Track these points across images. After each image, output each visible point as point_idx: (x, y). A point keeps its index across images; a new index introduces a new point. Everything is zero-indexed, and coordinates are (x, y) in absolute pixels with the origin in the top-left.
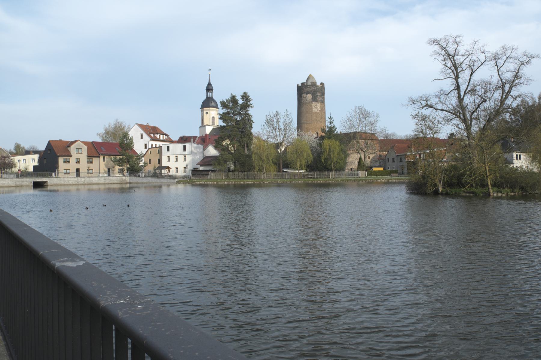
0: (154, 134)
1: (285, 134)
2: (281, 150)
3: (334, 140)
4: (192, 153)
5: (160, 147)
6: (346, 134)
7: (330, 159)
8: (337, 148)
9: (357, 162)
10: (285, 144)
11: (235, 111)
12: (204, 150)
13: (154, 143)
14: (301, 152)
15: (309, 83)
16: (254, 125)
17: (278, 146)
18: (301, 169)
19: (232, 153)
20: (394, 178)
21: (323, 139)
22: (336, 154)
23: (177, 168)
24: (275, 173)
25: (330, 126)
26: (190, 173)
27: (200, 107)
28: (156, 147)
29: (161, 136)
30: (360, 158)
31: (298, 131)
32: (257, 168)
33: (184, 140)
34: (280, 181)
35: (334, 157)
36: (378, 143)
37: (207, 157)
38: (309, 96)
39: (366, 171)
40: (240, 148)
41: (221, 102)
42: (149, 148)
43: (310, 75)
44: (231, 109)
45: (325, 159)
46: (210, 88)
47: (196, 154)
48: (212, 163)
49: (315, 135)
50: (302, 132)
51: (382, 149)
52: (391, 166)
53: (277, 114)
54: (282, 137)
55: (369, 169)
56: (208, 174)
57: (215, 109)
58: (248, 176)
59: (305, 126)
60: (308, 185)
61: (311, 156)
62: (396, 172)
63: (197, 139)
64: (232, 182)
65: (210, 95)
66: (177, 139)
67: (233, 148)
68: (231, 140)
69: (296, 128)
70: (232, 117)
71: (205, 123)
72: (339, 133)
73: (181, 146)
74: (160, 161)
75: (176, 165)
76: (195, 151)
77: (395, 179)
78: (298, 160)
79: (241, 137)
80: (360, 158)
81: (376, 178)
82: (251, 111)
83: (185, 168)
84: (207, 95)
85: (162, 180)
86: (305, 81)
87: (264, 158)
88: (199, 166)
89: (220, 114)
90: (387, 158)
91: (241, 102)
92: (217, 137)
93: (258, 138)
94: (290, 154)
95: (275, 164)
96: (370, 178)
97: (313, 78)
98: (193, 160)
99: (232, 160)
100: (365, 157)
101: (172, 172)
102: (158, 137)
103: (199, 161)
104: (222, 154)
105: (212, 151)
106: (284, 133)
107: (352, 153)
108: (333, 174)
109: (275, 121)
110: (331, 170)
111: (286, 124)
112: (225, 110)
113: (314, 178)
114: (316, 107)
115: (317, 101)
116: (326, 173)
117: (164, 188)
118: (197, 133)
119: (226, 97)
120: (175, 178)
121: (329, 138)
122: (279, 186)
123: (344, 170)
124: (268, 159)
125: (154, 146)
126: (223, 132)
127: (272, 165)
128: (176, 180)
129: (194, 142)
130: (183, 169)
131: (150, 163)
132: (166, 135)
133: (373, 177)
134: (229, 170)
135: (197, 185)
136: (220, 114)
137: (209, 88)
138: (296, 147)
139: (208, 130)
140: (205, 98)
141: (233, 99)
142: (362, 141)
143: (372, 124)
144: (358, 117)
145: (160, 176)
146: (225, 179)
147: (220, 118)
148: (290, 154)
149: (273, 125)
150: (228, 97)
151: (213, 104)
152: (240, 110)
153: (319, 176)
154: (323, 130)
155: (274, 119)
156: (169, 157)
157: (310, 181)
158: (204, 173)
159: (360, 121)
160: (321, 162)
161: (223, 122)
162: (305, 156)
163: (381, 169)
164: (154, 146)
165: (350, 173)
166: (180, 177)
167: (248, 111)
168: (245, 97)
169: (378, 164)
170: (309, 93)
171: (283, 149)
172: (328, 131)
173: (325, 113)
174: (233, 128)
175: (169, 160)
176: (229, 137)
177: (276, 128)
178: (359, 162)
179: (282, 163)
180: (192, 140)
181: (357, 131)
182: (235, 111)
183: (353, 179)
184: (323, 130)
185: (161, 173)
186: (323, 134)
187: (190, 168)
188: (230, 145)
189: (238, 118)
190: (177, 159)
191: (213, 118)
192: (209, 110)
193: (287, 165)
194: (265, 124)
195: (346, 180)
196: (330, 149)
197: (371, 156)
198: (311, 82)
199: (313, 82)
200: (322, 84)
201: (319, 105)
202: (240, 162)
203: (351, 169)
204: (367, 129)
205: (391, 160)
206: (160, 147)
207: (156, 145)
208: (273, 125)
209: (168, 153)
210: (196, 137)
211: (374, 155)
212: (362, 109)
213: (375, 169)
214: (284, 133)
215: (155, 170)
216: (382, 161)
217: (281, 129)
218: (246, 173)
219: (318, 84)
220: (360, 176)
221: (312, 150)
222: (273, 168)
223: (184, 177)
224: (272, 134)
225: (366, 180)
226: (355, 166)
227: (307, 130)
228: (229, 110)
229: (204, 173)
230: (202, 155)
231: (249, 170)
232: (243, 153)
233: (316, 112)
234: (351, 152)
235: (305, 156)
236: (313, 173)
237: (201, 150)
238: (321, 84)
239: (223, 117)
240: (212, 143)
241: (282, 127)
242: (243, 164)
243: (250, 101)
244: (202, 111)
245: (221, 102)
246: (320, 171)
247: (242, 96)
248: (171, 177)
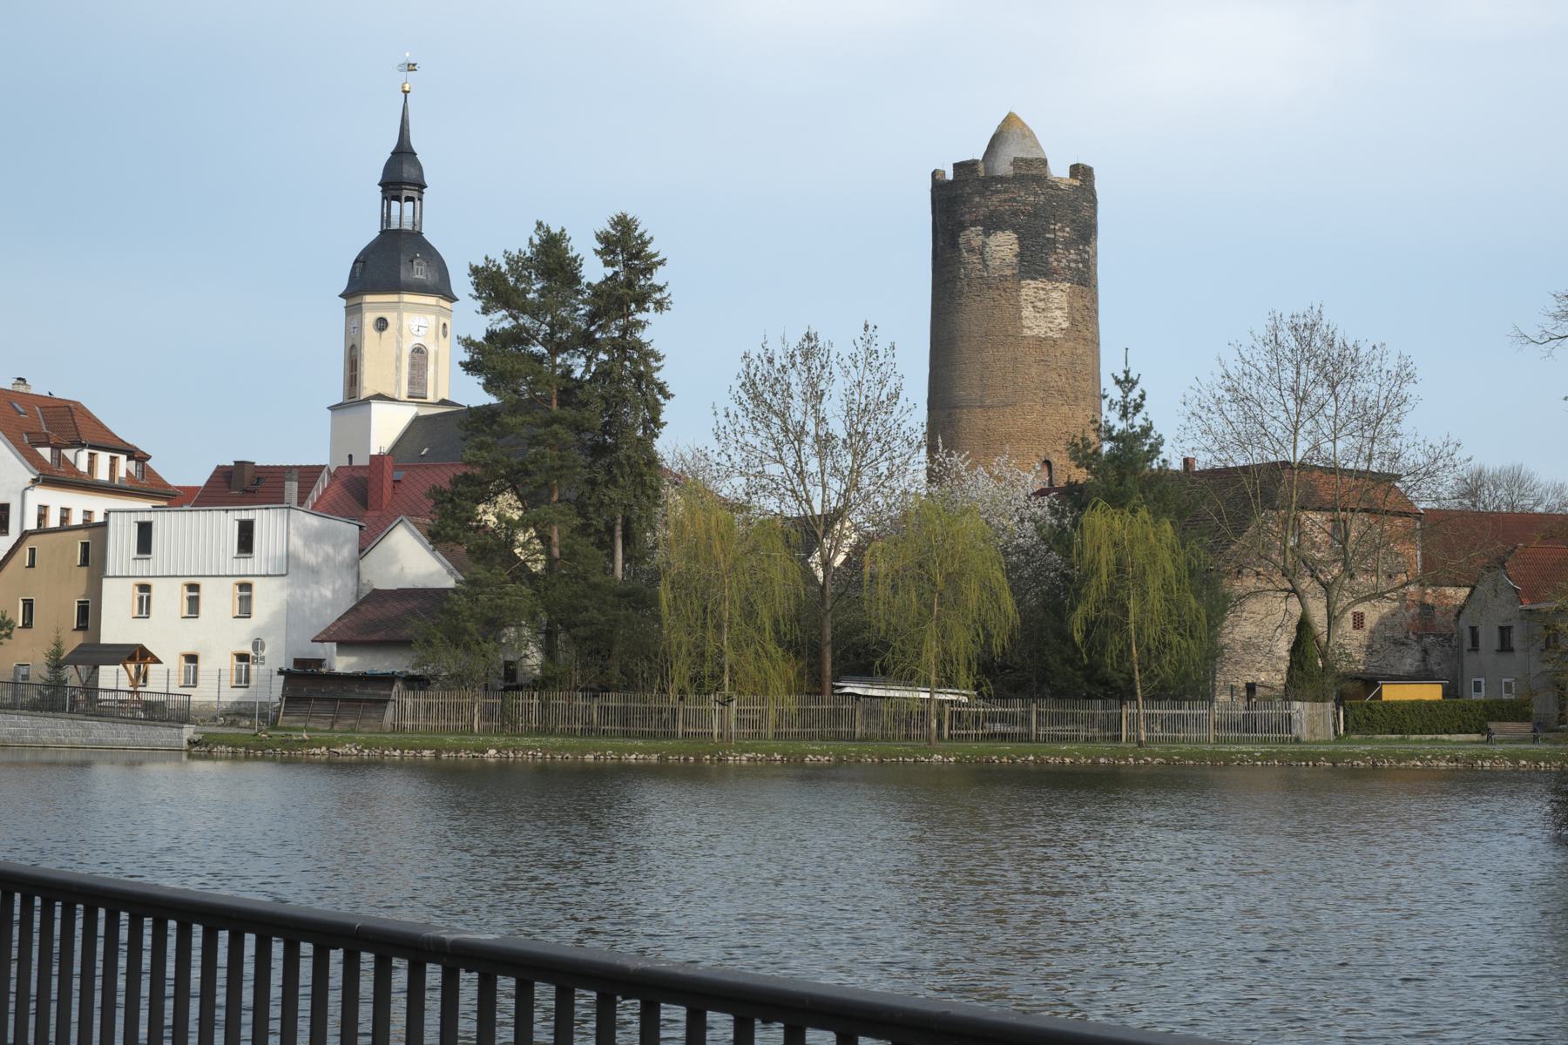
0: (56, 448)
1: (856, 472)
2: (826, 564)
3: (1143, 513)
4: (290, 567)
5: (97, 530)
6: (1223, 477)
7: (1121, 627)
8: (1165, 556)
9: (1283, 647)
10: (857, 528)
11: (558, 325)
12: (363, 549)
13: (56, 499)
14: (948, 577)
15: (1004, 167)
16: (669, 412)
17: (809, 532)
18: (949, 682)
19: (533, 577)
20: (1506, 745)
21: (1080, 505)
22: (1155, 597)
23: (192, 658)
24: (791, 704)
25: (1120, 426)
26: (268, 688)
27: (343, 284)
28: (65, 526)
29: (103, 458)
30: (1304, 625)
31: (932, 450)
32: (681, 671)
33: (241, 486)
34: (818, 754)
35: (1145, 611)
36: (1408, 537)
37: (378, 596)
38: (1004, 246)
39: (1339, 702)
40: (585, 545)
41: (475, 271)
42: (25, 535)
43: (1010, 120)
44: (535, 311)
45: (1090, 626)
46: (408, 172)
47: (313, 572)
48: (407, 632)
49: (1034, 479)
50: (959, 461)
51: (1432, 574)
52: (1493, 678)
53: (809, 349)
54: (836, 485)
55: (1357, 693)
56: (383, 702)
57: (431, 300)
58: (625, 717)
59: (973, 421)
60: (986, 776)
61: (1008, 602)
62: (1515, 711)
63: (323, 482)
64: (532, 751)
65: (403, 214)
66: (198, 477)
67: (537, 545)
68: (528, 500)
69: (920, 435)
70: (539, 359)
71: (368, 387)
72: (1177, 465)
73: (226, 522)
74: (88, 615)
75: (190, 636)
76: (310, 558)
77: (1515, 758)
78: (931, 628)
79: (592, 483)
80: (1304, 625)
81: (1400, 749)
82: (655, 329)
83: (242, 657)
84: (386, 218)
85: (101, 731)
86: (977, 153)
87: (726, 611)
88: (328, 651)
89: (468, 344)
90: (1464, 624)
91: (594, 271)
92: (442, 472)
93: (693, 486)
94: (883, 591)
95: (793, 648)
96: (1363, 747)
97: (1027, 135)
98: (292, 610)
99: (533, 616)
100: (1332, 619)
101: (161, 681)
102: (83, 466)
103: (331, 616)
104: (472, 582)
105: (410, 559)
106: (847, 461)
107: (1257, 593)
108: (1139, 717)
109: (796, 390)
110: (1125, 693)
111: (860, 413)
112: (500, 320)
113: (1025, 738)
114: (1043, 310)
115: (1049, 274)
116: (1098, 709)
117: (106, 775)
118: (311, 445)
119: (509, 241)
120: (181, 715)
121: (1117, 500)
122: (813, 776)
123: (1208, 697)
124: (750, 614)
125: (54, 521)
126: (481, 446)
127: (771, 647)
128: (188, 732)
129: (301, 502)
130: (229, 664)
131: (28, 624)
132: (132, 453)
133: (1384, 742)
134: (511, 678)
135: (310, 763)
136: (468, 344)
137: (401, 177)
138: (920, 539)
139: (387, 427)
140: (372, 232)
141: (551, 256)
142: (1315, 521)
143: (1372, 420)
144: (1289, 375)
145: (90, 704)
146: (486, 731)
147: (470, 367)
148: (883, 591)
149: (782, 415)
150: (520, 241)
151: (420, 273)
152: (592, 317)
153: (1059, 730)
154: (1081, 453)
155: (793, 377)
156: (145, 588)
157: (1001, 755)
158: (364, 693)
159: (1302, 400)
160: (1067, 638)
161: (488, 387)
162: (973, 603)
163: (1431, 692)
164: (54, 521)
165: (1241, 711)
166: (211, 716)
167: (640, 325)
168: (624, 242)
169: (1410, 662)
170: (1006, 223)
171: (840, 559)
172: (1112, 457)
173: (1094, 343)
174: (548, 424)
175: (144, 607)
176: (514, 480)
177: (800, 434)
178: (1297, 649)
179: (836, 640)
180: (292, 488)
181: (1287, 455)
182: (558, 325)
183: (1259, 750)
184: (1081, 453)
185: (91, 688)
186: (1081, 475)
187: (277, 657)
188: (524, 524)
189: (579, 366)
190: (194, 606)
191: (429, 353)
192: (394, 306)
193: (864, 660)
194: (734, 407)
195: (1215, 756)
196: (1120, 567)
197: (1373, 613)
198: (1016, 162)
199: (1028, 162)
200: (1081, 172)
201: (1059, 295)
202: (582, 632)
203: (1251, 688)
204: (1344, 450)
205: (1489, 639)
206: (97, 530)
207: (66, 512)
208: (782, 415)
209: (142, 567)
210: (318, 469)
211: (1385, 607)
212: (1312, 327)
213: (1392, 693)
214: (847, 461)
215: (57, 664)
216: (1433, 641)
217: (830, 438)
218: (614, 700)
219: (1059, 170)
220: (1301, 730)
221: (1015, 568)
222: (782, 670)
223: (236, 713)
224: (774, 470)
225: (1334, 758)
226: (1272, 675)
227: (989, 446)
228: (525, 320)
229: (357, 691)
230: (351, 583)
231: (630, 684)
232: (597, 579)
233: (1040, 341)
234: (1251, 583)
235: (973, 603)
236: (1016, 707)
237: (348, 551)
238: (1076, 170)
239: (485, 359)
240: (413, 513)
241: (838, 428)
242: (597, 647)
243: (649, 270)
244: (353, 311)
245: (475, 271)
246: (1060, 694)
247: (604, 238)
248: (156, 712)
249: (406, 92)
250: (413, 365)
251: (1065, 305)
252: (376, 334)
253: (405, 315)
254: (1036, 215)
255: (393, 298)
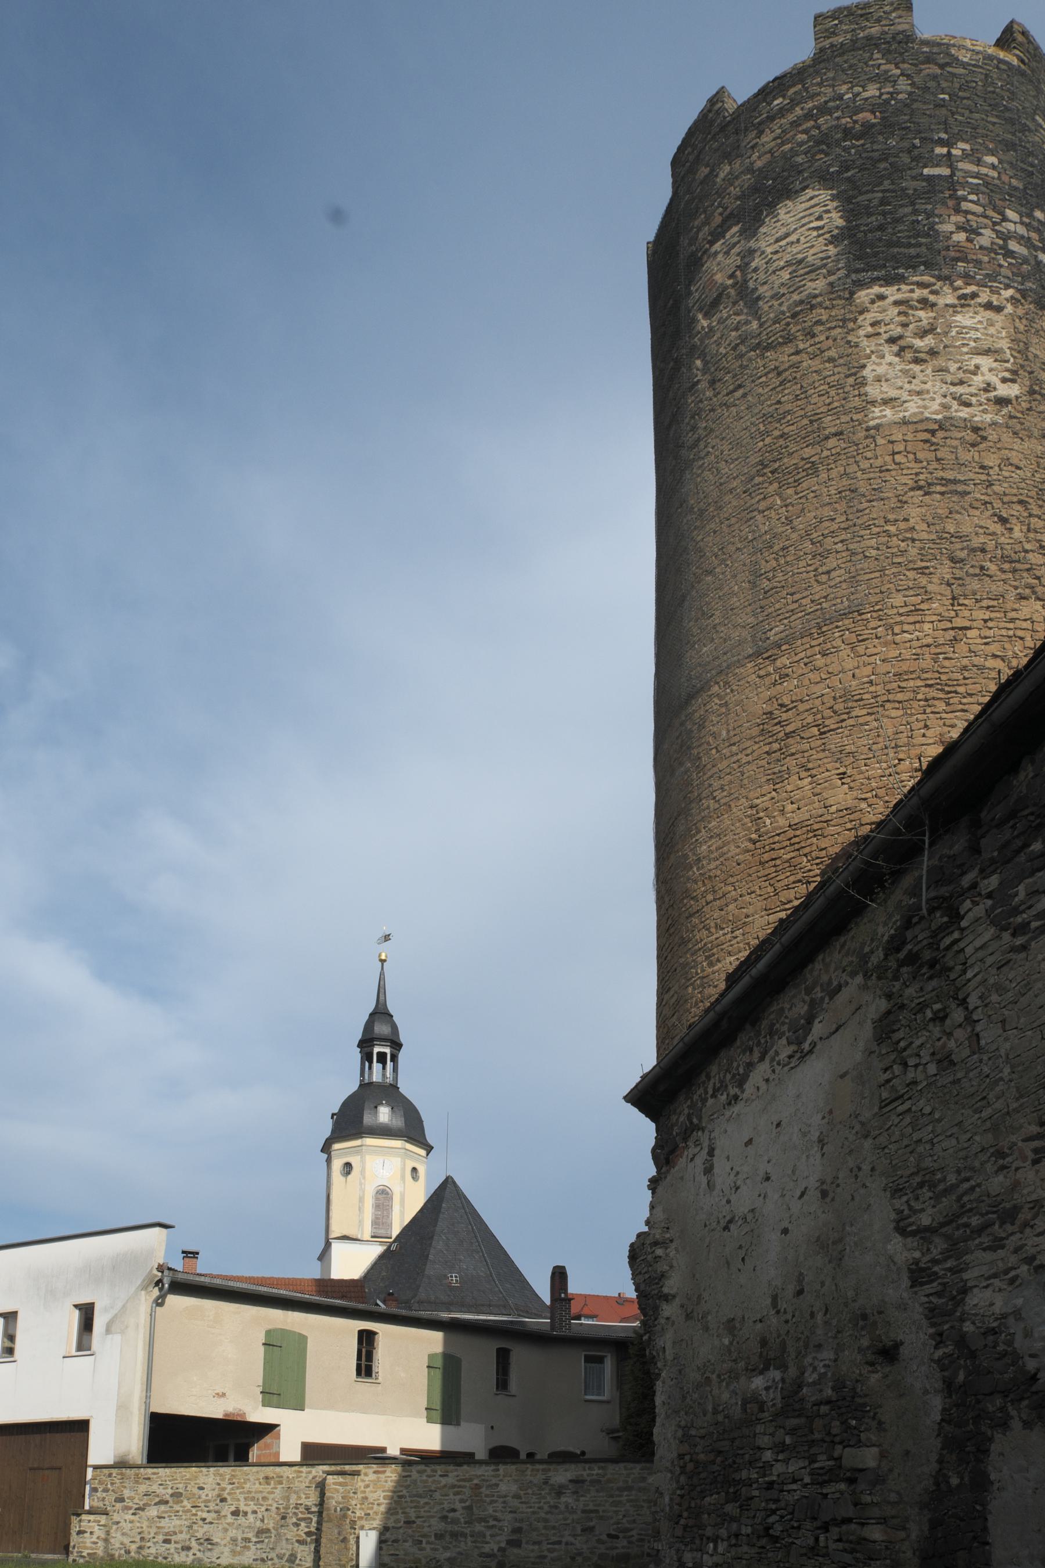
57: (398, 1143)
115: (931, 258)
137: (379, 1037)
140: (353, 1086)
249: (383, 961)
250: (377, 1207)
251: (1004, 344)
252: (343, 1179)
253: (368, 1157)
254: (887, 126)
255: (358, 1142)
